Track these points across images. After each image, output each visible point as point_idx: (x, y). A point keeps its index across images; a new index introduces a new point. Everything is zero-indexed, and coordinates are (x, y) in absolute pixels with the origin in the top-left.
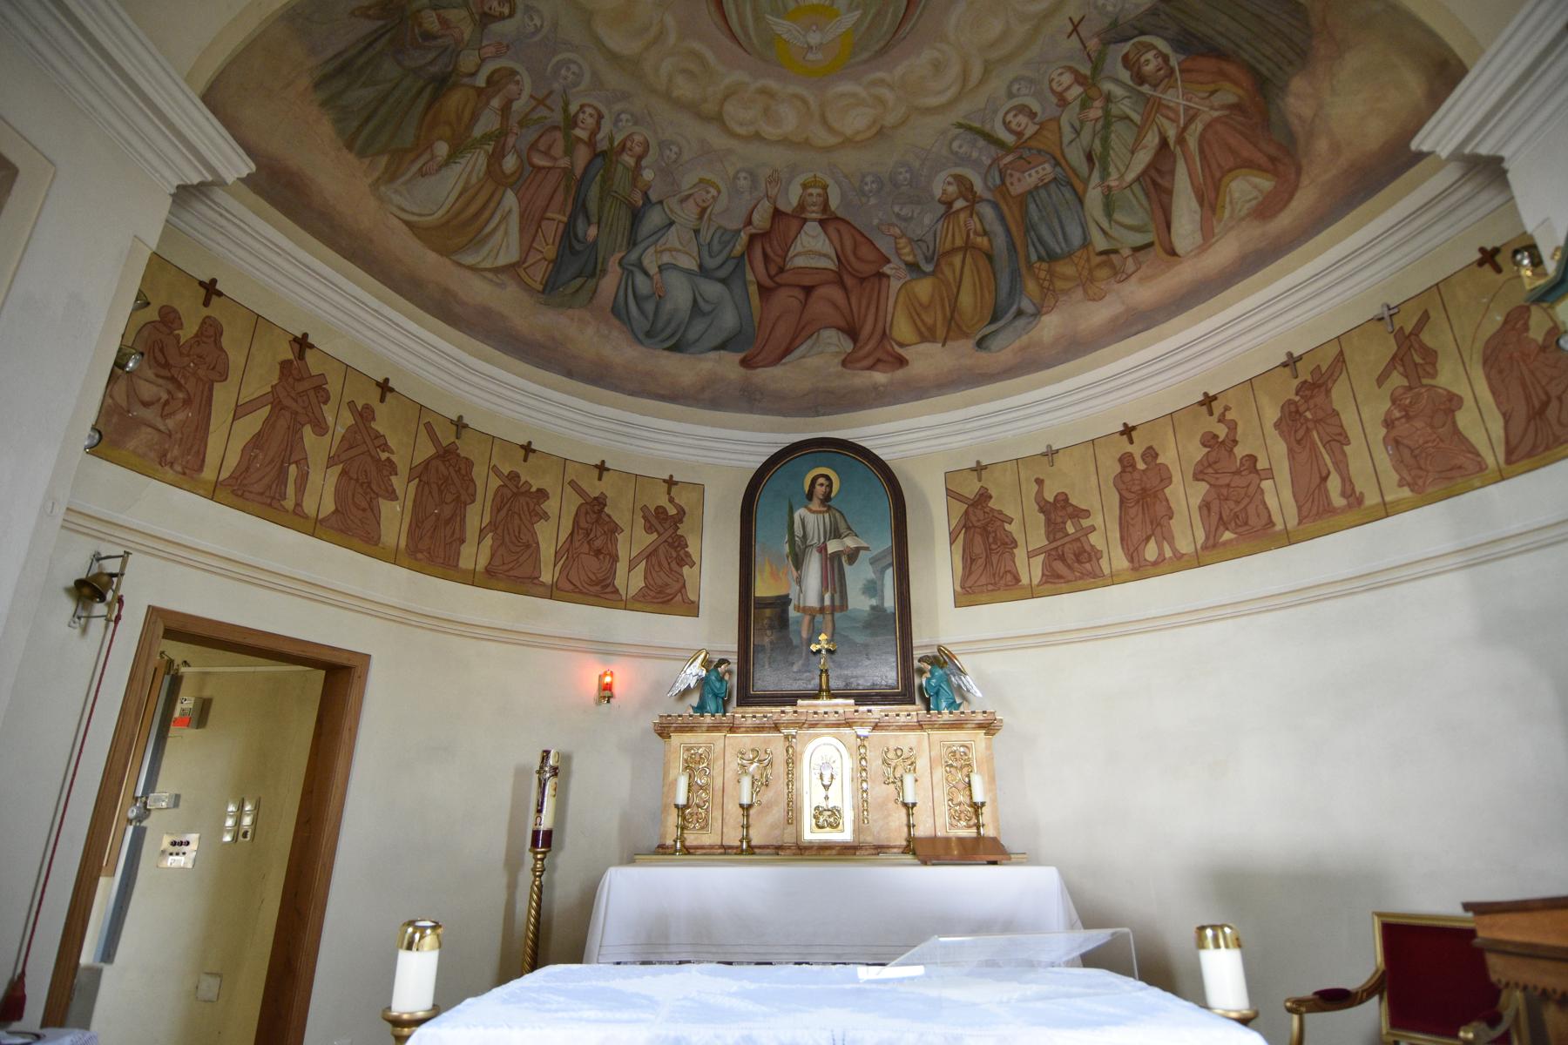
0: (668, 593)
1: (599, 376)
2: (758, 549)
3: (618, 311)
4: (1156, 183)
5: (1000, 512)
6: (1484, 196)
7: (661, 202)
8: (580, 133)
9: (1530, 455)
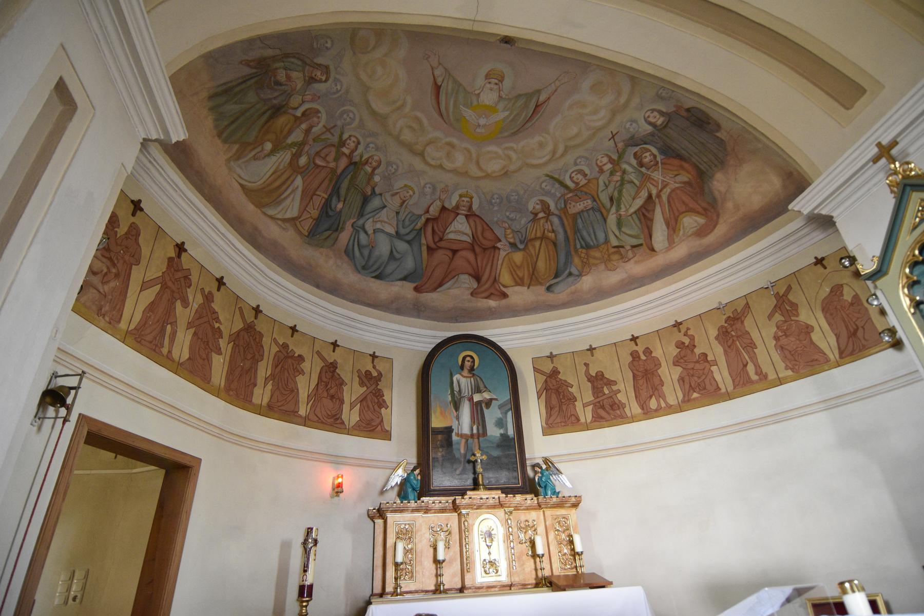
0: (373, 426)
1: (333, 289)
2: (432, 398)
3: (348, 253)
4: (645, 215)
5: (566, 381)
6: (814, 234)
7: (381, 194)
8: (345, 150)
9: (851, 354)
